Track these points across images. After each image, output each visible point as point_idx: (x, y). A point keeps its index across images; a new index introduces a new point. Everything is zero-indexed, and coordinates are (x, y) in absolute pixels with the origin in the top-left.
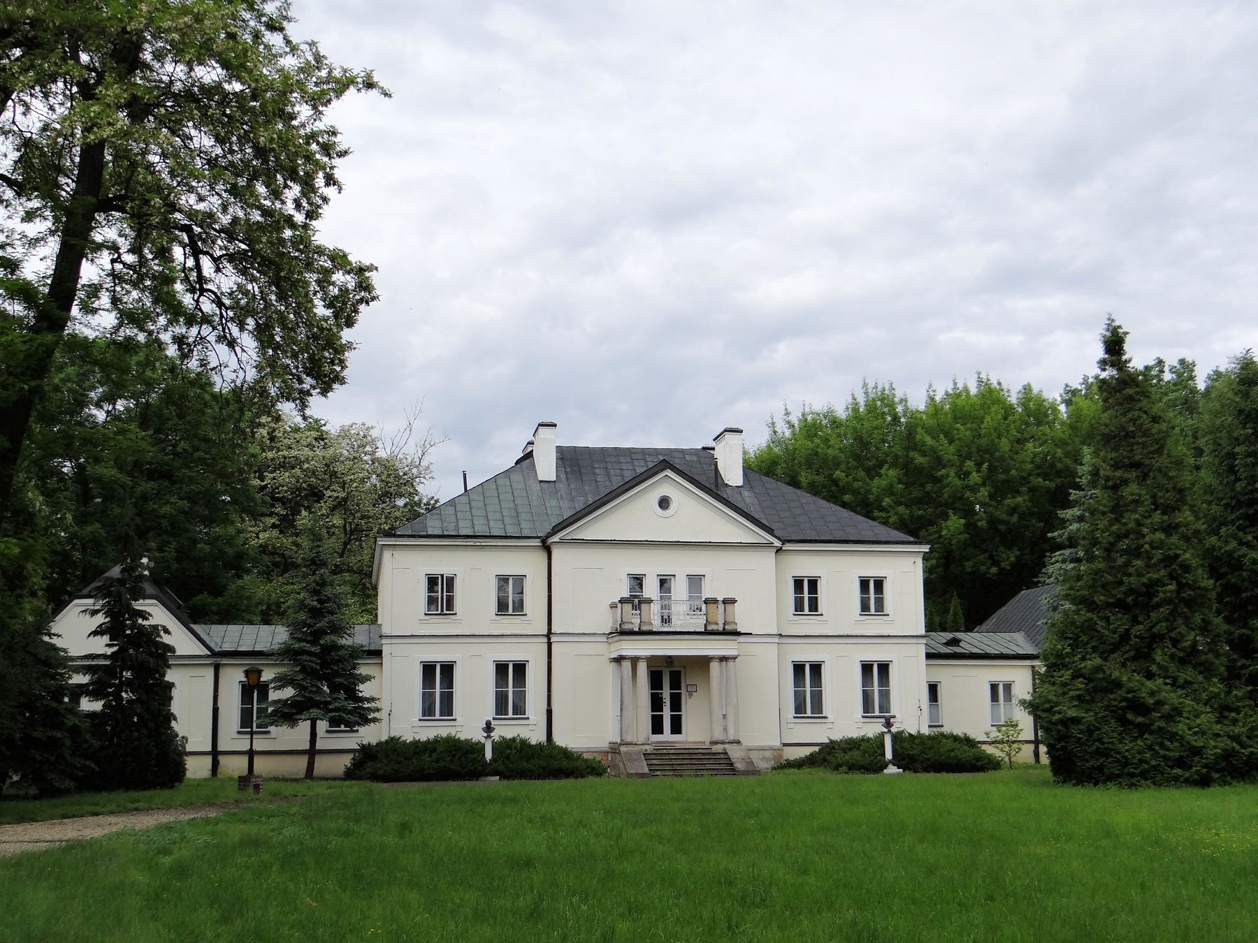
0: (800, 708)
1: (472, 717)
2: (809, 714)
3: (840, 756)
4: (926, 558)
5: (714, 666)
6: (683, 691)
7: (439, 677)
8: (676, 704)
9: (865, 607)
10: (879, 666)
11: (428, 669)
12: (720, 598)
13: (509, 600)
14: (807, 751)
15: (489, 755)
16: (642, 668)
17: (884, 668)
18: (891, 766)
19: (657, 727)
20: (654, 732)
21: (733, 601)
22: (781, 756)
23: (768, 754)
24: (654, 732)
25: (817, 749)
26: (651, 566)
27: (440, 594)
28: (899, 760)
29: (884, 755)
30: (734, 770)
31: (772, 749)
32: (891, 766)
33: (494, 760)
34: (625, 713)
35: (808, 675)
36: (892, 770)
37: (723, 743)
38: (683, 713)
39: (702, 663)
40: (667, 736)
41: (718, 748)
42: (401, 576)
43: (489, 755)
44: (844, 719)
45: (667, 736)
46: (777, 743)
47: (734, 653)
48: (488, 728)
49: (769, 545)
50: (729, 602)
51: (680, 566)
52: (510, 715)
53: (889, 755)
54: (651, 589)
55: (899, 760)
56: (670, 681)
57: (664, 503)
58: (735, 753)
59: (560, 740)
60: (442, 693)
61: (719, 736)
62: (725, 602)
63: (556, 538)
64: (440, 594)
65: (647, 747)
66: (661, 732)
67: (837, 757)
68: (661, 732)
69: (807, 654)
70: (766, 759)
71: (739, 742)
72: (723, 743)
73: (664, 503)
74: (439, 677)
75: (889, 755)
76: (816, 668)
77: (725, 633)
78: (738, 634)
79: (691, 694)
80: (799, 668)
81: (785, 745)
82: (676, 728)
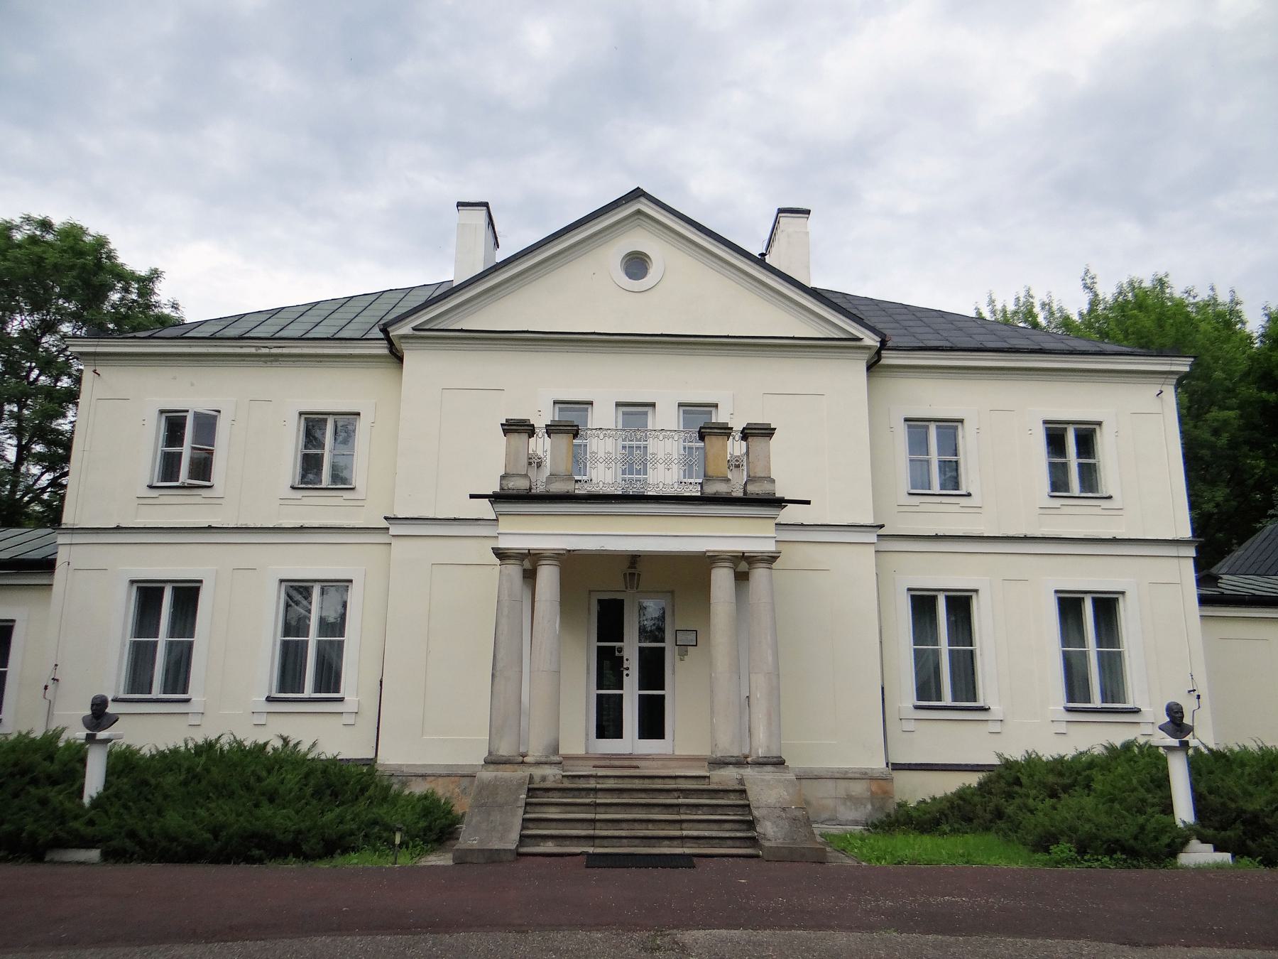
0: (927, 688)
1: (233, 699)
2: (947, 700)
3: (1043, 814)
4: (1182, 382)
5: (722, 579)
6: (668, 645)
7: (167, 608)
8: (653, 672)
9: (1058, 483)
10: (1095, 601)
11: (148, 595)
12: (738, 425)
13: (320, 451)
14: (948, 785)
15: (94, 781)
16: (548, 576)
17: (1107, 606)
18: (1195, 843)
19: (608, 724)
20: (601, 734)
21: (767, 432)
22: (887, 794)
23: (859, 788)
24: (601, 734)
25: (973, 779)
26: (602, 384)
27: (186, 451)
28: (1216, 820)
29: (1168, 808)
30: (753, 841)
31: (865, 776)
32: (1195, 843)
33: (97, 803)
34: (497, 680)
35: (943, 617)
36: (1200, 855)
37: (740, 762)
38: (667, 692)
39: (691, 572)
40: (630, 742)
41: (727, 776)
42: (115, 417)
43: (94, 781)
44: (1027, 713)
45: (630, 742)
46: (877, 764)
47: (769, 547)
48: (99, 715)
49: (843, 345)
50: (758, 432)
51: (670, 385)
52: (308, 692)
53: (1184, 811)
54: (603, 416)
55: (1216, 820)
56: (630, 621)
57: (637, 264)
58: (767, 792)
59: (591, 751)
60: (170, 646)
61: (727, 746)
62: (748, 433)
63: (405, 329)
64: (186, 451)
65: (549, 771)
66: (619, 735)
67: (1008, 799)
68: (619, 735)
69: (943, 574)
70: (850, 799)
71: (779, 763)
72: (740, 762)
73: (637, 264)
74: (167, 608)
75: (1184, 811)
76: (961, 605)
77: (747, 501)
78: (780, 503)
79: (683, 649)
80: (923, 604)
81: (897, 767)
82: (652, 725)
